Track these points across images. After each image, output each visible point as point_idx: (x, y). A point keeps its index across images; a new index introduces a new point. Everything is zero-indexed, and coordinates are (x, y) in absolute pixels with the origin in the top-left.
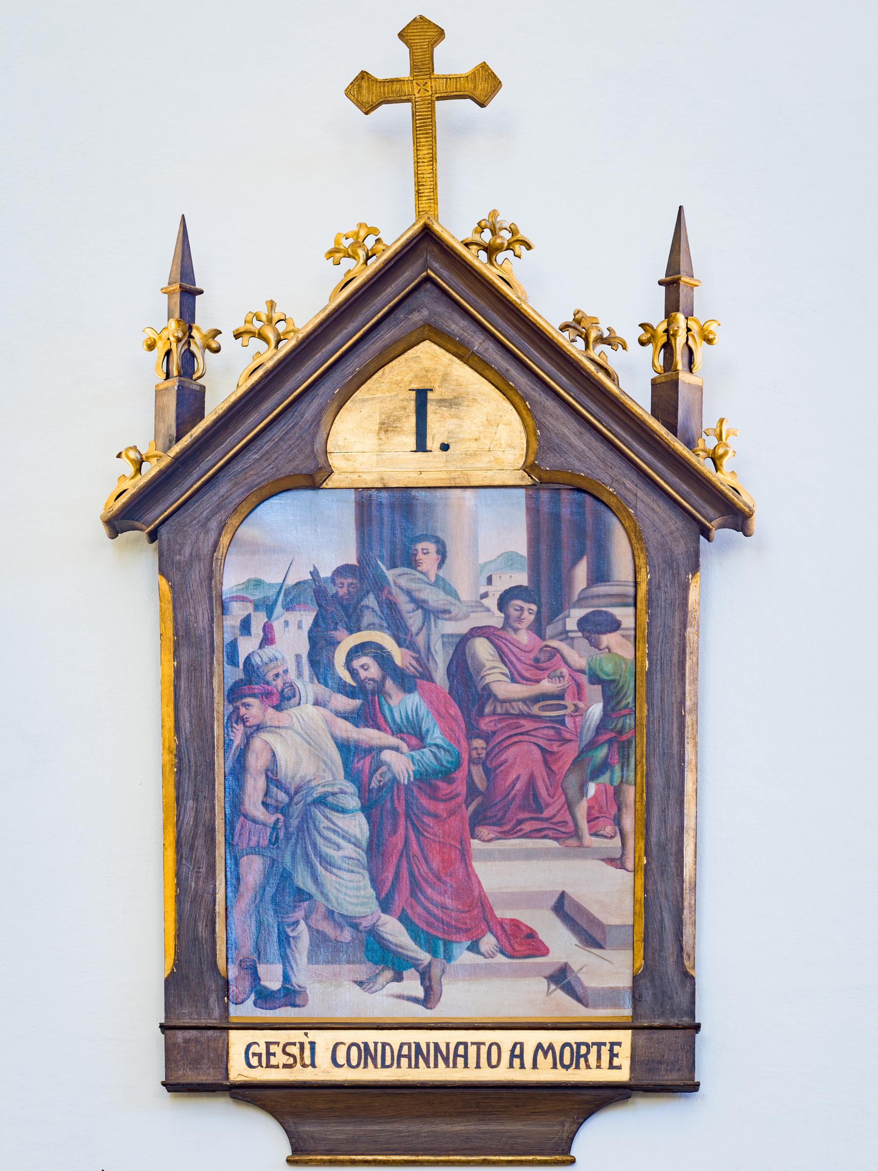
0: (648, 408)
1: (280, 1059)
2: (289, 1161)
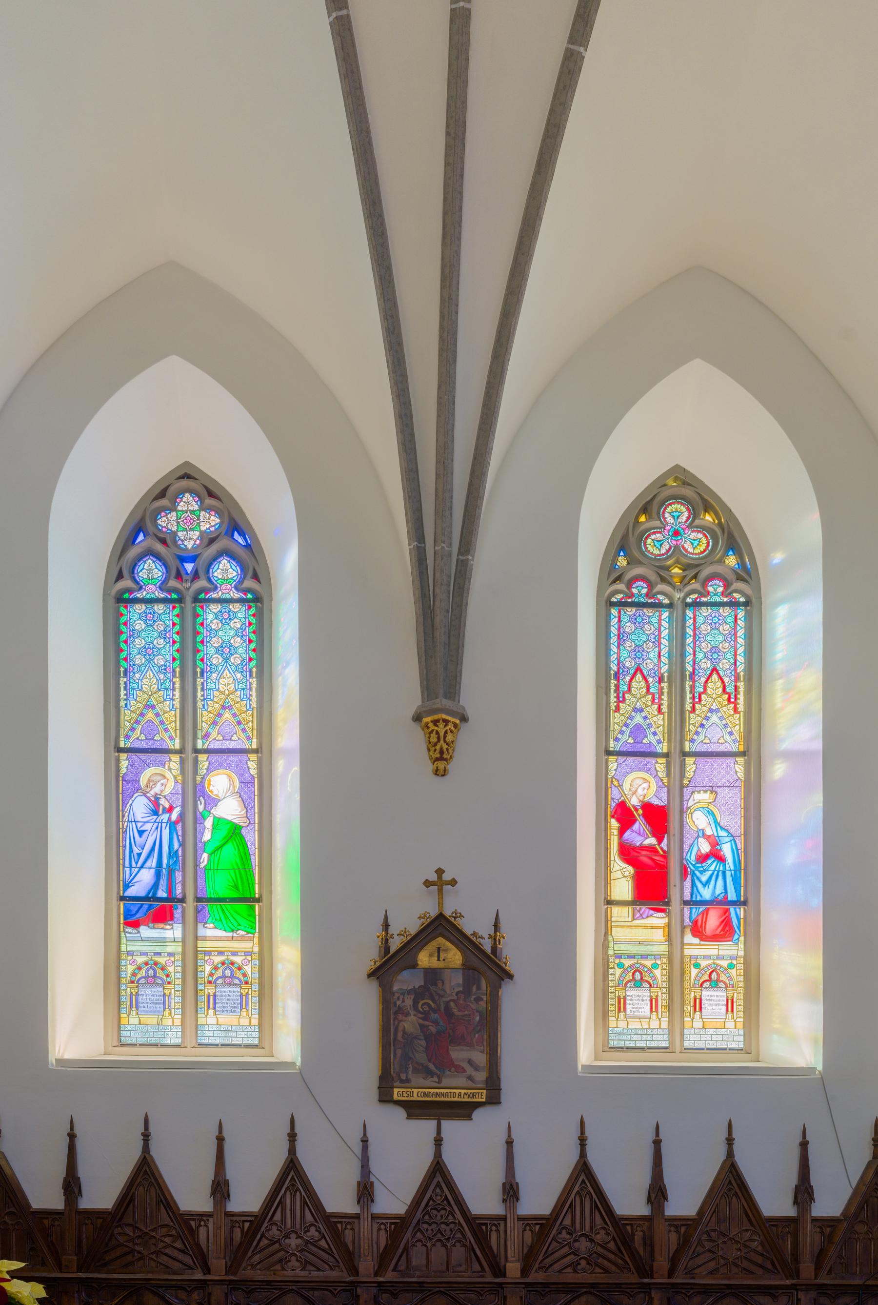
2: (407, 1118)
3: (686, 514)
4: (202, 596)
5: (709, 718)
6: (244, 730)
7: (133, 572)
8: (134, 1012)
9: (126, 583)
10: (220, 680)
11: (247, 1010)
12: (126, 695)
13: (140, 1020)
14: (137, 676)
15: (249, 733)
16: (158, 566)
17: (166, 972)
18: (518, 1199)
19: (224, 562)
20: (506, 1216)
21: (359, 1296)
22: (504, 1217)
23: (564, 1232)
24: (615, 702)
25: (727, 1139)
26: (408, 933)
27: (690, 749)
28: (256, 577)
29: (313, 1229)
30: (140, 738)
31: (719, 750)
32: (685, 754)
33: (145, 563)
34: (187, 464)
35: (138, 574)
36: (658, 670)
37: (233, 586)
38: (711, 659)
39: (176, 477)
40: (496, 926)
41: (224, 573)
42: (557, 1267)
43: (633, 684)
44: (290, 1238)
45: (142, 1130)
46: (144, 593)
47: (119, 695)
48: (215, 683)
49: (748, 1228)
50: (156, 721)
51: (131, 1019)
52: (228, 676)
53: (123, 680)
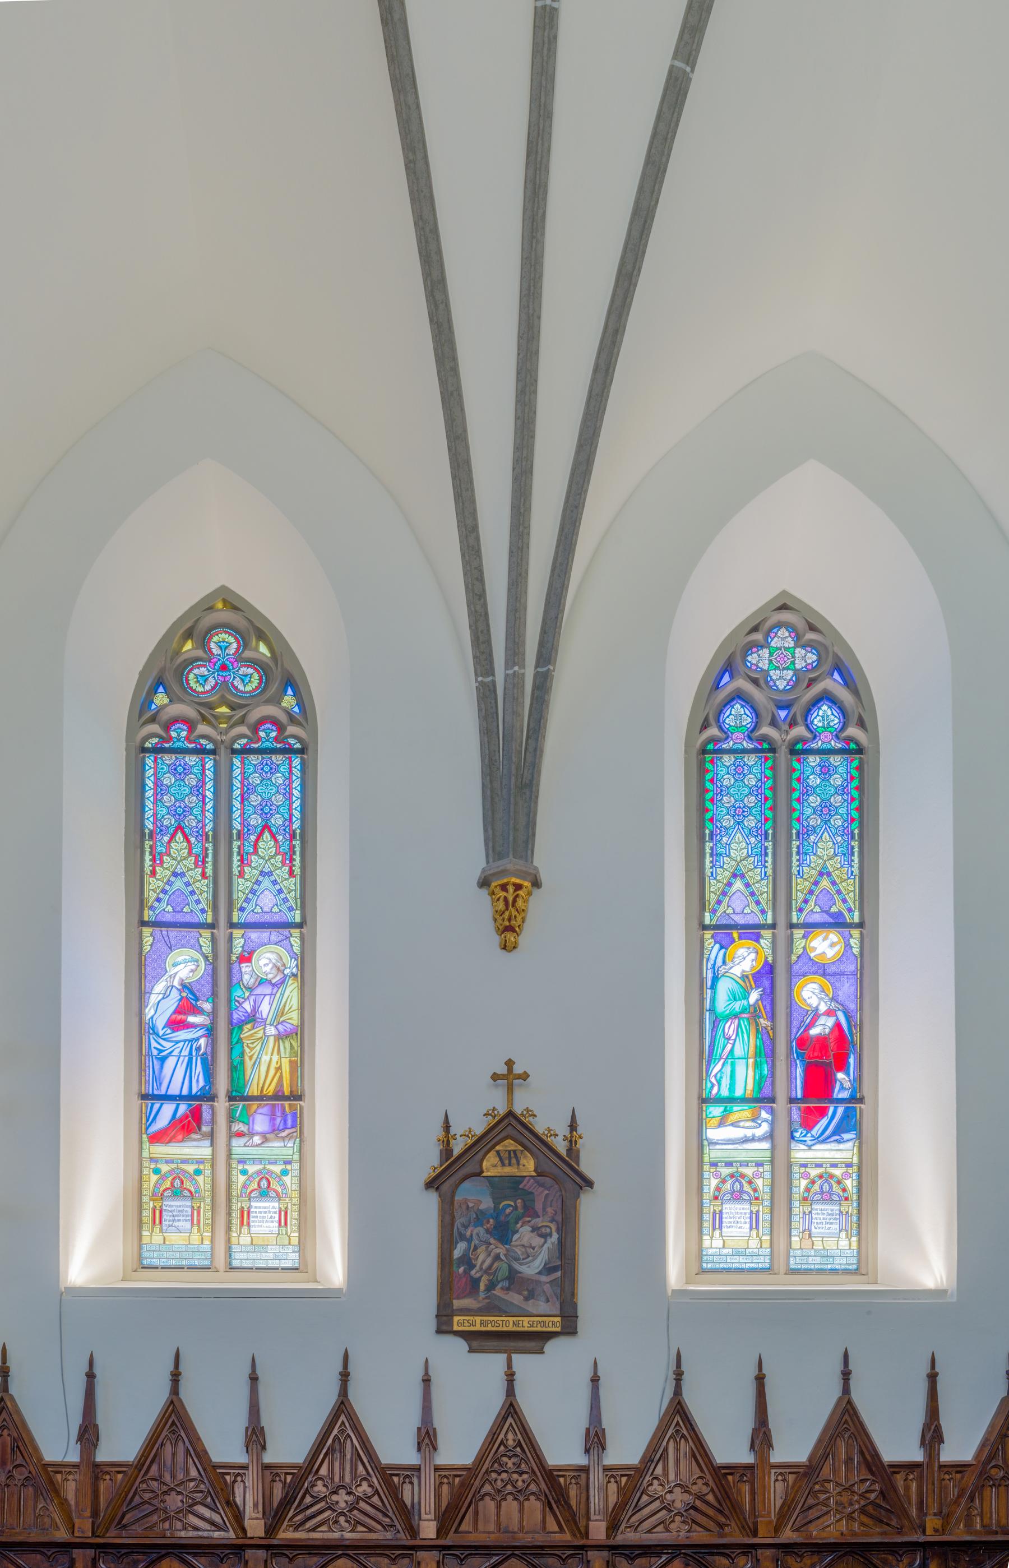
0: (565, 1154)
1: (467, 1324)
2: (469, 1352)
3: (235, 645)
4: (711, 747)
5: (261, 882)
6: (758, 903)
7: (806, 720)
8: (157, 1228)
9: (713, 731)
10: (819, 844)
11: (199, 1227)
12: (798, 860)
13: (164, 1239)
14: (725, 839)
15: (292, 903)
16: (747, 712)
17: (753, 1186)
18: (604, 1448)
19: (738, 708)
20: (420, 1465)
21: (74, 1559)
22: (418, 1467)
23: (656, 1482)
24: (150, 866)
25: (341, 1374)
26: (473, 1133)
27: (239, 920)
28: (861, 724)
29: (365, 1484)
30: (814, 910)
31: (184, 920)
32: (792, 926)
33: (733, 707)
34: (784, 593)
35: (724, 721)
36: (202, 828)
37: (745, 735)
38: (175, 815)
39: (774, 608)
40: (573, 1126)
41: (737, 719)
42: (647, 1525)
43: (260, 844)
44: (338, 1494)
45: (171, 1367)
46: (731, 743)
47: (791, 862)
48: (726, 847)
49: (868, 1478)
50: (833, 890)
51: (153, 1238)
52: (741, 840)
53: (708, 845)
